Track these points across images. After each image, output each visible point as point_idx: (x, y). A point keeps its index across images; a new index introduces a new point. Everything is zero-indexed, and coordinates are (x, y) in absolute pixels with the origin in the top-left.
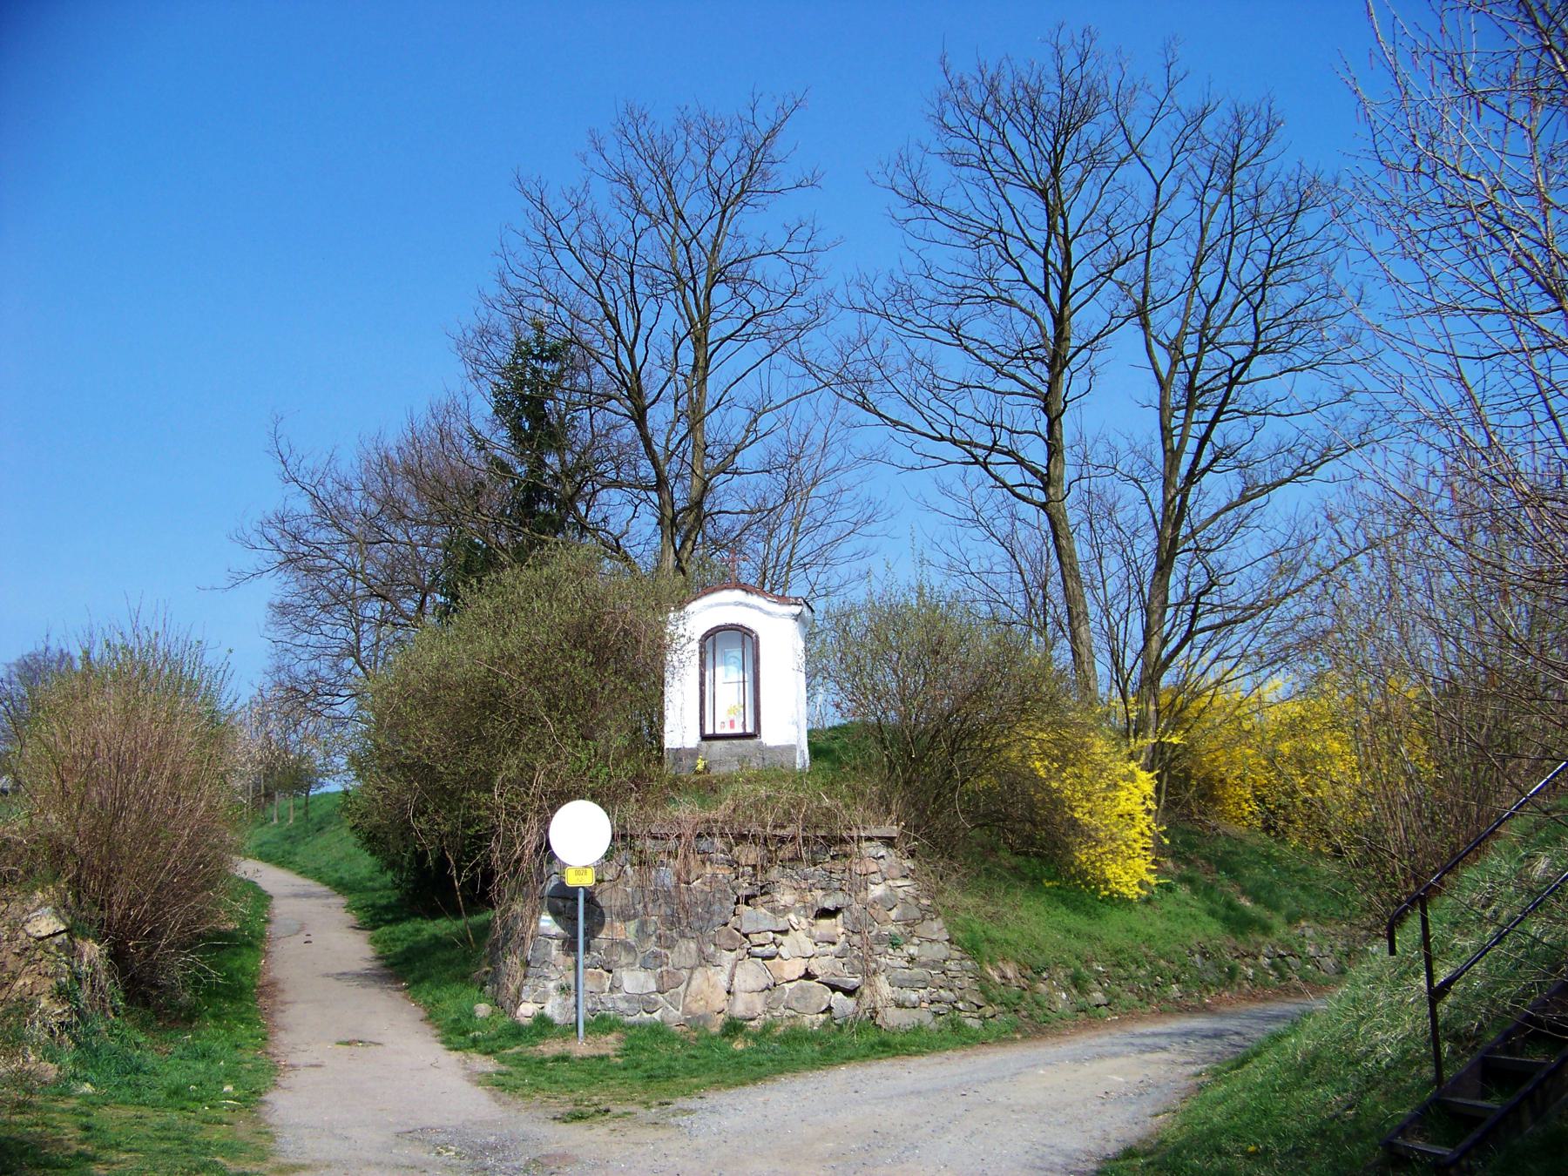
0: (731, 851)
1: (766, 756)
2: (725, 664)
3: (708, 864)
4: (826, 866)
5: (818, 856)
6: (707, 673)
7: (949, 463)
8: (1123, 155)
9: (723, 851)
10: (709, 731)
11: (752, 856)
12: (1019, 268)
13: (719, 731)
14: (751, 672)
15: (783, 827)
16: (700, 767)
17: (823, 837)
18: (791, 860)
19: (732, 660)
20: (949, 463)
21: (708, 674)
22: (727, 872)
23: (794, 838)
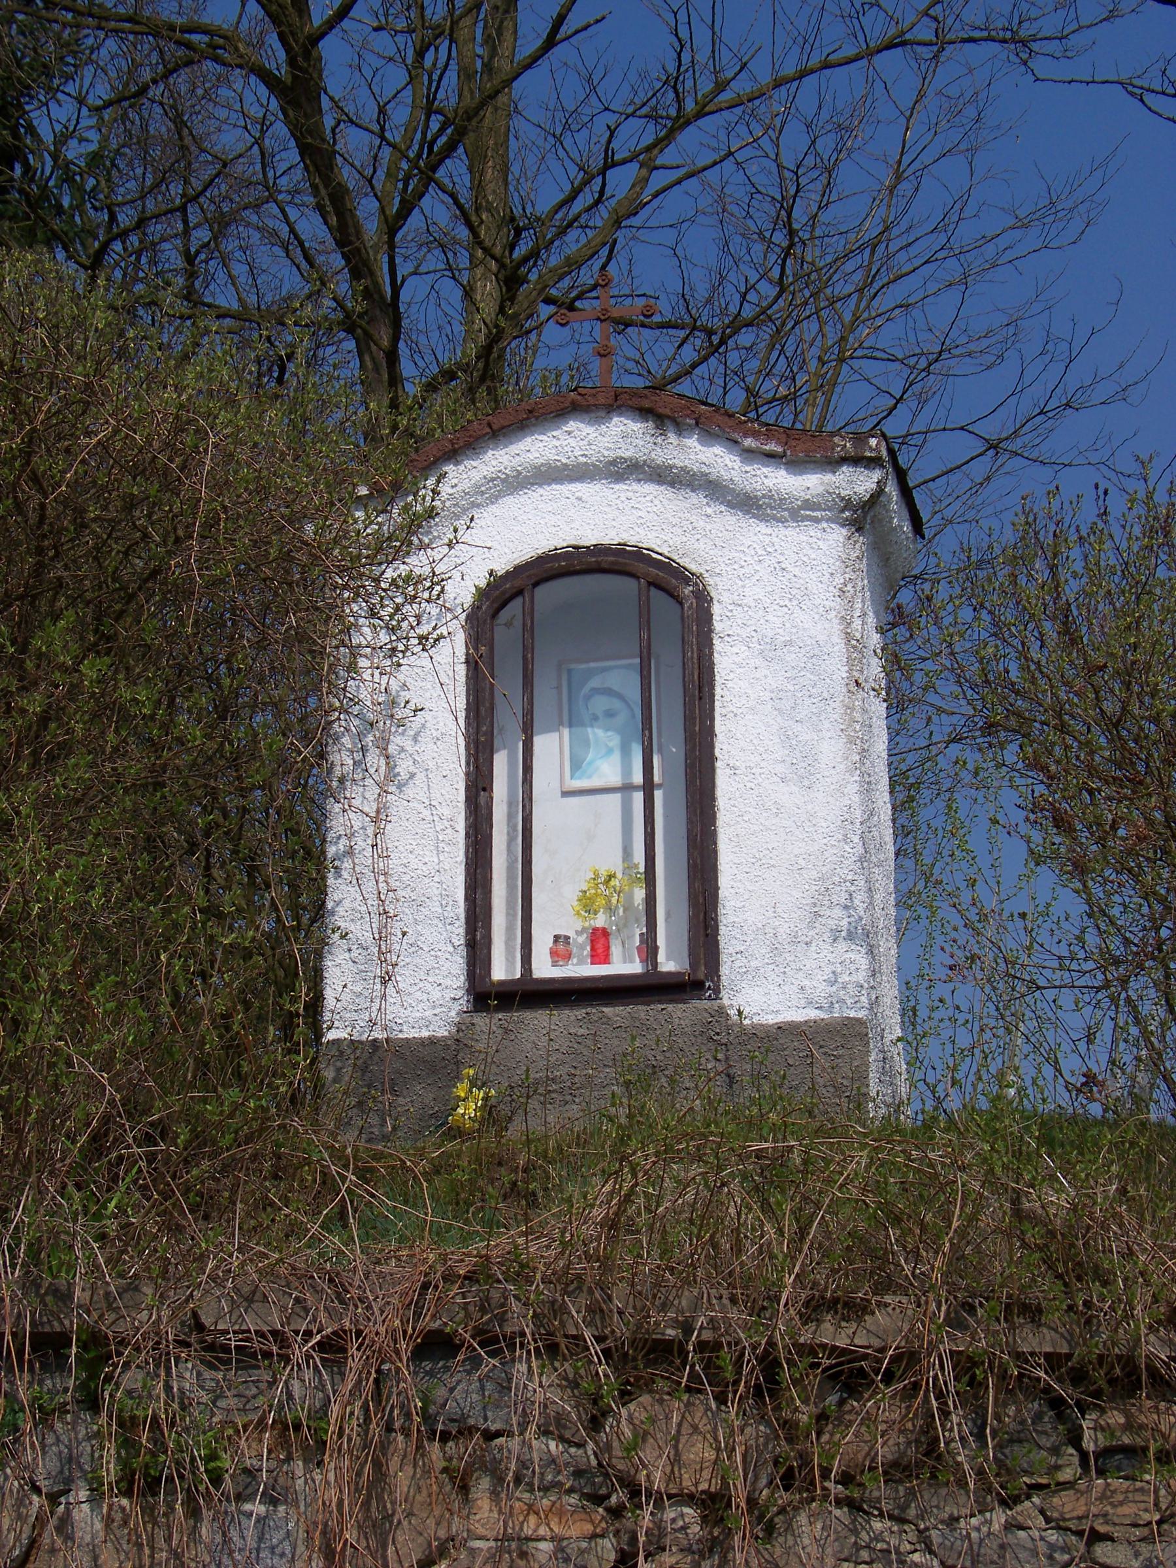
0: (595, 1424)
1: (742, 1069)
2: (572, 719)
3: (482, 1486)
4: (1066, 1504)
5: (1020, 1455)
6: (500, 762)
7: (962, 428)
8: (785, 244)
9: (554, 1426)
10: (502, 969)
11: (699, 1451)
12: (921, 96)
13: (544, 969)
14: (676, 750)
15: (854, 1310)
16: (468, 1111)
17: (1053, 1361)
18: (897, 1470)
19: (600, 704)
20: (962, 428)
21: (502, 765)
22: (577, 1529)
23: (908, 1358)
